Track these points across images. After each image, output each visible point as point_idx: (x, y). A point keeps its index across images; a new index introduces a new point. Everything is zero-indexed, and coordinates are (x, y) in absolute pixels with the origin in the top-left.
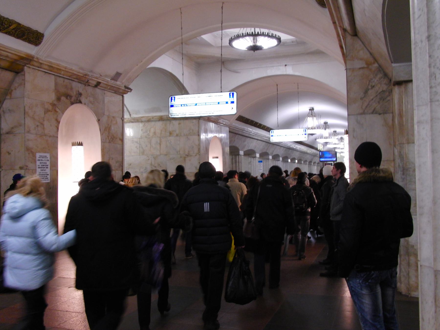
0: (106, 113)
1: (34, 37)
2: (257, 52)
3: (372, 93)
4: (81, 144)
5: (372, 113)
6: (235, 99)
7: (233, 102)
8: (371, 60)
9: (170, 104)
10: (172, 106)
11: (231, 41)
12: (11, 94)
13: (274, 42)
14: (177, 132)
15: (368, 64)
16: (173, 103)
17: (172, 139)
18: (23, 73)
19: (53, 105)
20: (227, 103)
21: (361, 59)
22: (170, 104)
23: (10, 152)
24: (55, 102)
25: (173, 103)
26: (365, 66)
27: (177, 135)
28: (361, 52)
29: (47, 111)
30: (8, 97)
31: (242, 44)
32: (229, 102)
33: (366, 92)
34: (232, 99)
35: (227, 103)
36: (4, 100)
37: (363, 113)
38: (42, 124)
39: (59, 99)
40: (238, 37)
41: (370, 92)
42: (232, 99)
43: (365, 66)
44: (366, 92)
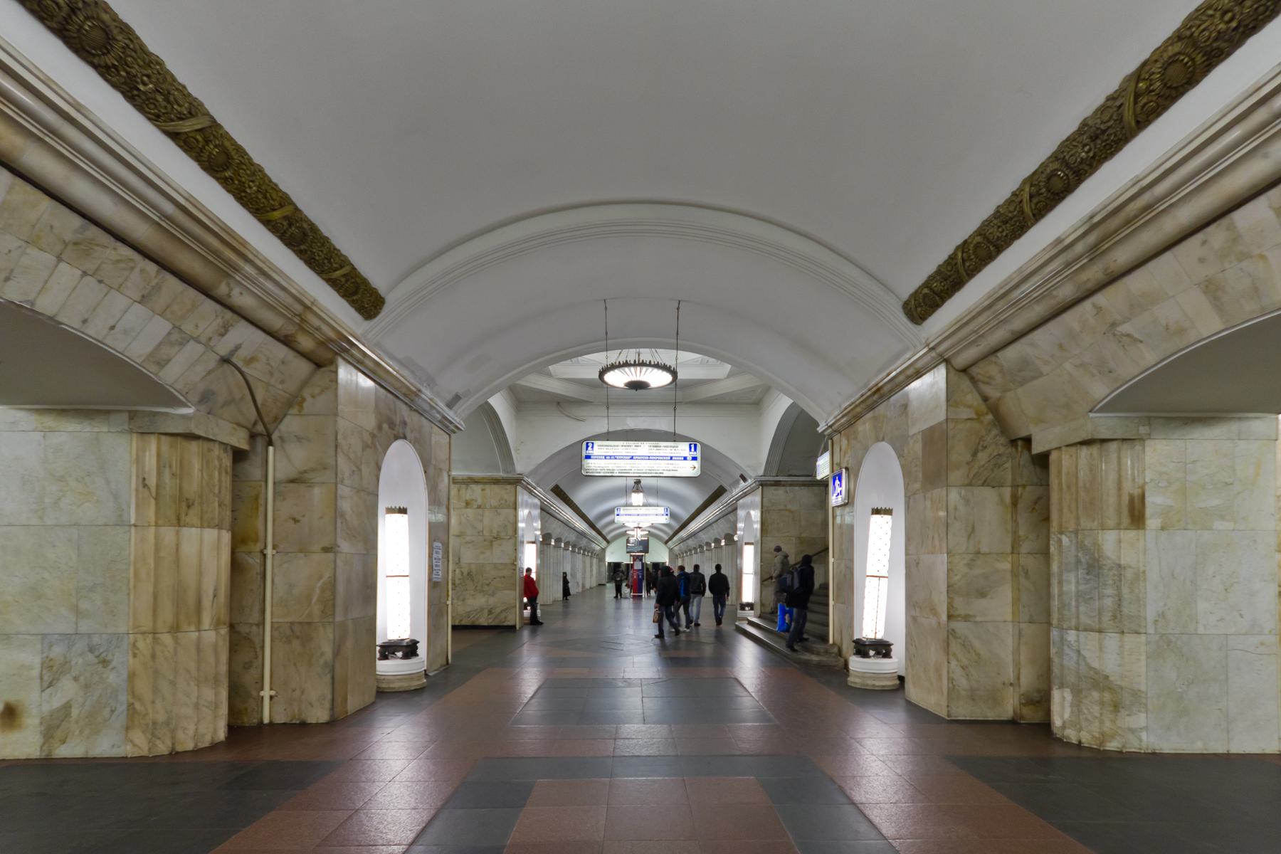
0: (433, 462)
1: (366, 300)
2: (640, 392)
3: (983, 456)
4: (403, 511)
5: (983, 485)
6: (698, 454)
7: (694, 459)
8: (983, 408)
9: (584, 454)
10: (588, 457)
11: (602, 373)
12: (300, 405)
13: (666, 378)
14: (480, 502)
15: (979, 415)
16: (590, 451)
17: (470, 512)
18: (332, 368)
19: (373, 436)
20: (685, 458)
21: (969, 407)
22: (584, 454)
23: (298, 517)
24: (376, 432)
25: (590, 451)
26: (974, 416)
27: (479, 507)
28: (969, 396)
29: (366, 446)
30: (294, 411)
31: (617, 379)
32: (689, 458)
33: (975, 454)
34: (693, 454)
35: (685, 458)
36: (285, 416)
37: (970, 484)
38: (360, 470)
39: (380, 428)
40: (613, 367)
41: (980, 455)
42: (693, 454)
43: (974, 416)
44: (975, 454)
